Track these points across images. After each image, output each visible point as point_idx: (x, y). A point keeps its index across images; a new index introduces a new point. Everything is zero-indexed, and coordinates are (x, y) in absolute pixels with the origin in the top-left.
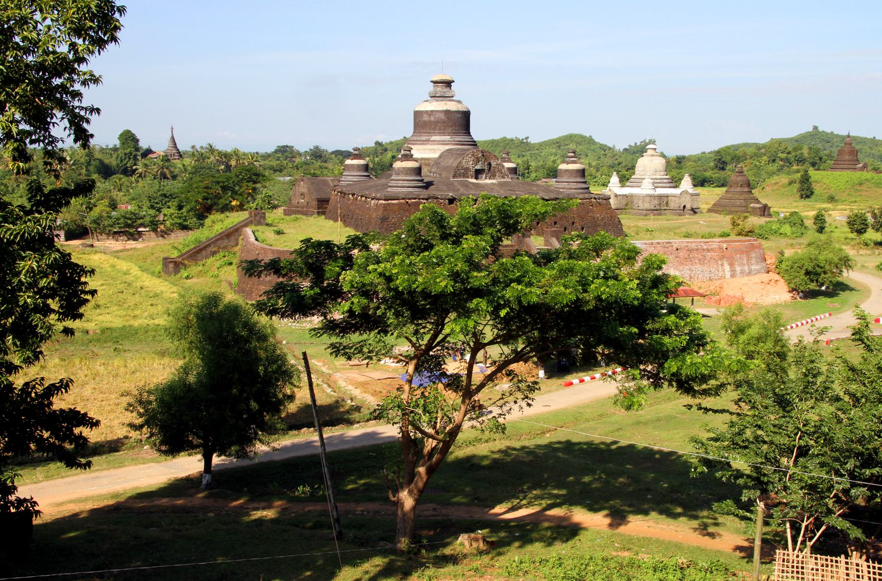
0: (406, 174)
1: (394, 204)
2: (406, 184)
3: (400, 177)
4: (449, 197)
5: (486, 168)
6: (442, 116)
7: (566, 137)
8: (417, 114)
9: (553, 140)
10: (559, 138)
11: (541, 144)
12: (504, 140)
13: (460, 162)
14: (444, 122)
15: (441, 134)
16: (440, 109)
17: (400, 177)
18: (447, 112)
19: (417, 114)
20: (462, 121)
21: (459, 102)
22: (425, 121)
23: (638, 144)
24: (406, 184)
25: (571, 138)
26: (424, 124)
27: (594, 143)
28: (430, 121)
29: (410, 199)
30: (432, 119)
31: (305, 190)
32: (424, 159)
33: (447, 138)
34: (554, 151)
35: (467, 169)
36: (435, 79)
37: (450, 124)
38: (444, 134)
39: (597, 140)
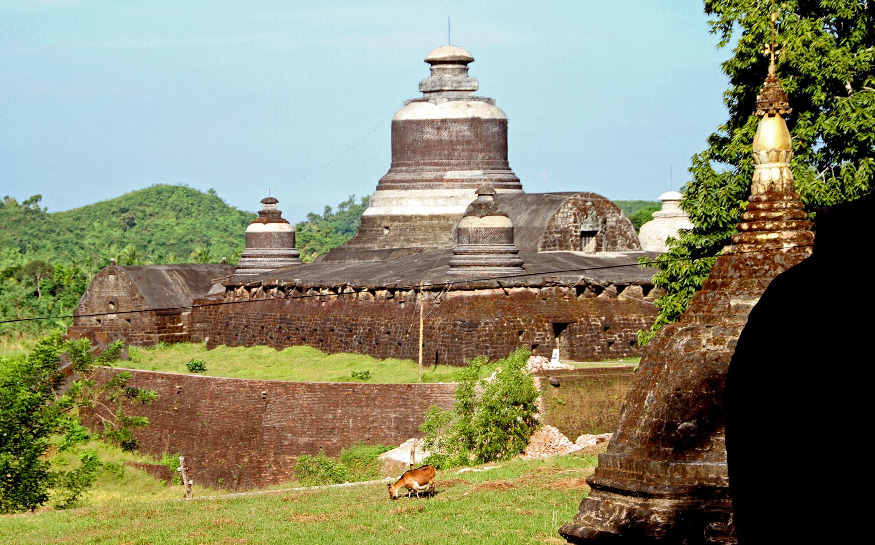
0: (493, 240)
1: (485, 298)
2: (494, 259)
3: (479, 247)
4: (577, 283)
5: (600, 229)
6: (466, 131)
7: (146, 193)
8: (399, 129)
9: (110, 204)
10: (127, 198)
11: (78, 216)
12: (87, 207)
13: (553, 219)
14: (469, 142)
15: (460, 166)
16: (461, 115)
17: (479, 247)
18: (475, 122)
19: (399, 129)
20: (491, 141)
21: (489, 101)
22: (428, 141)
23: (335, 211)
24: (494, 259)
25: (159, 195)
26: (411, 149)
27: (225, 210)
28: (441, 141)
29: (511, 287)
30: (445, 136)
31: (121, 294)
32: (438, 217)
33: (477, 173)
34: (117, 233)
35: (565, 232)
36: (431, 57)
37: (480, 146)
38: (469, 166)
39: (230, 202)
